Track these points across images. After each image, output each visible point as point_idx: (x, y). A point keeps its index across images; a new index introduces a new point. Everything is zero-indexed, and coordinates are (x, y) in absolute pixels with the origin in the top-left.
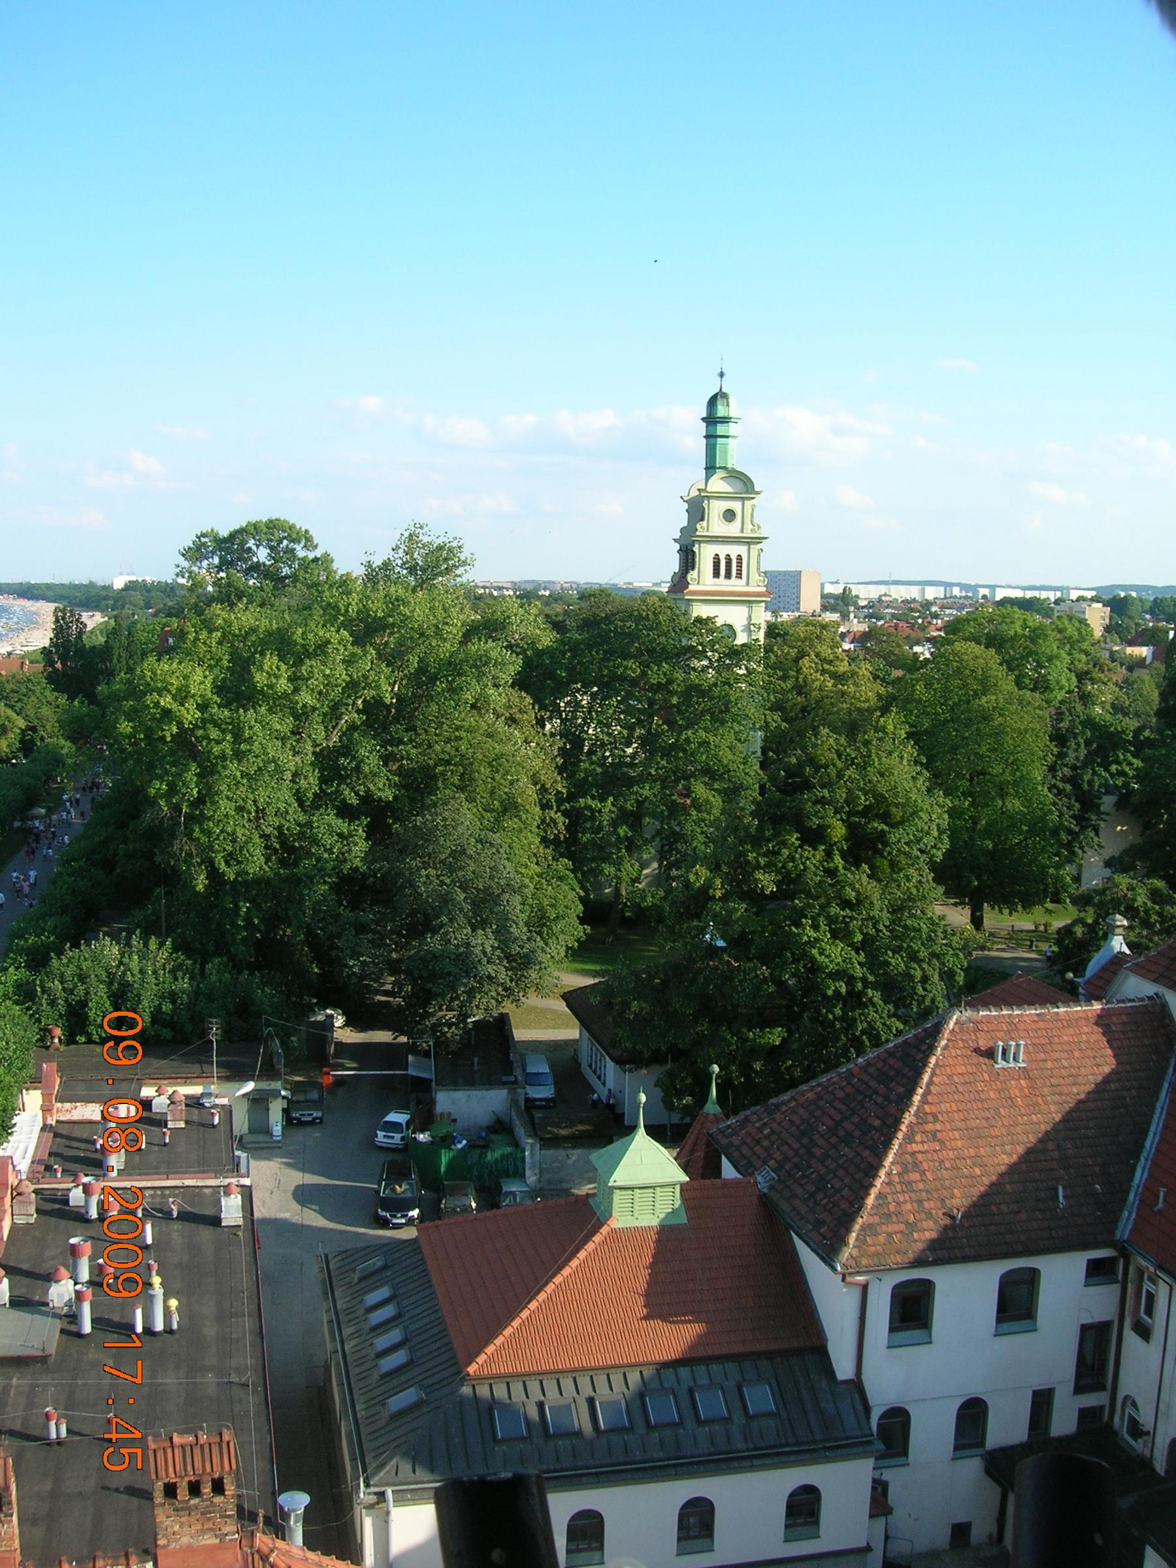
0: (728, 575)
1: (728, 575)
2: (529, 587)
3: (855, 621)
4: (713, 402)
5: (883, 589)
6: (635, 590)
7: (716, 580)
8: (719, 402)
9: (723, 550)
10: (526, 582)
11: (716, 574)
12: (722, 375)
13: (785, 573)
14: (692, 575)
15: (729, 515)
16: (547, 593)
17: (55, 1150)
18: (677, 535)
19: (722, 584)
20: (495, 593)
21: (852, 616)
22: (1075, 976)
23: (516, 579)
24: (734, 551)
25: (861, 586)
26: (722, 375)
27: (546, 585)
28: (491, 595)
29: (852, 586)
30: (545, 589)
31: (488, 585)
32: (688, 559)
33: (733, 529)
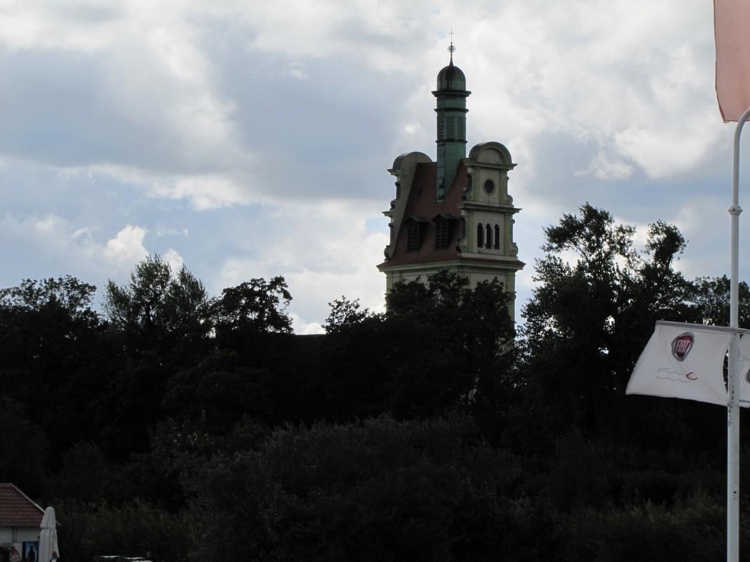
7: (480, 249)
11: (480, 244)
12: (451, 49)
17: (459, 114)
26: (451, 49)
33: (494, 200)
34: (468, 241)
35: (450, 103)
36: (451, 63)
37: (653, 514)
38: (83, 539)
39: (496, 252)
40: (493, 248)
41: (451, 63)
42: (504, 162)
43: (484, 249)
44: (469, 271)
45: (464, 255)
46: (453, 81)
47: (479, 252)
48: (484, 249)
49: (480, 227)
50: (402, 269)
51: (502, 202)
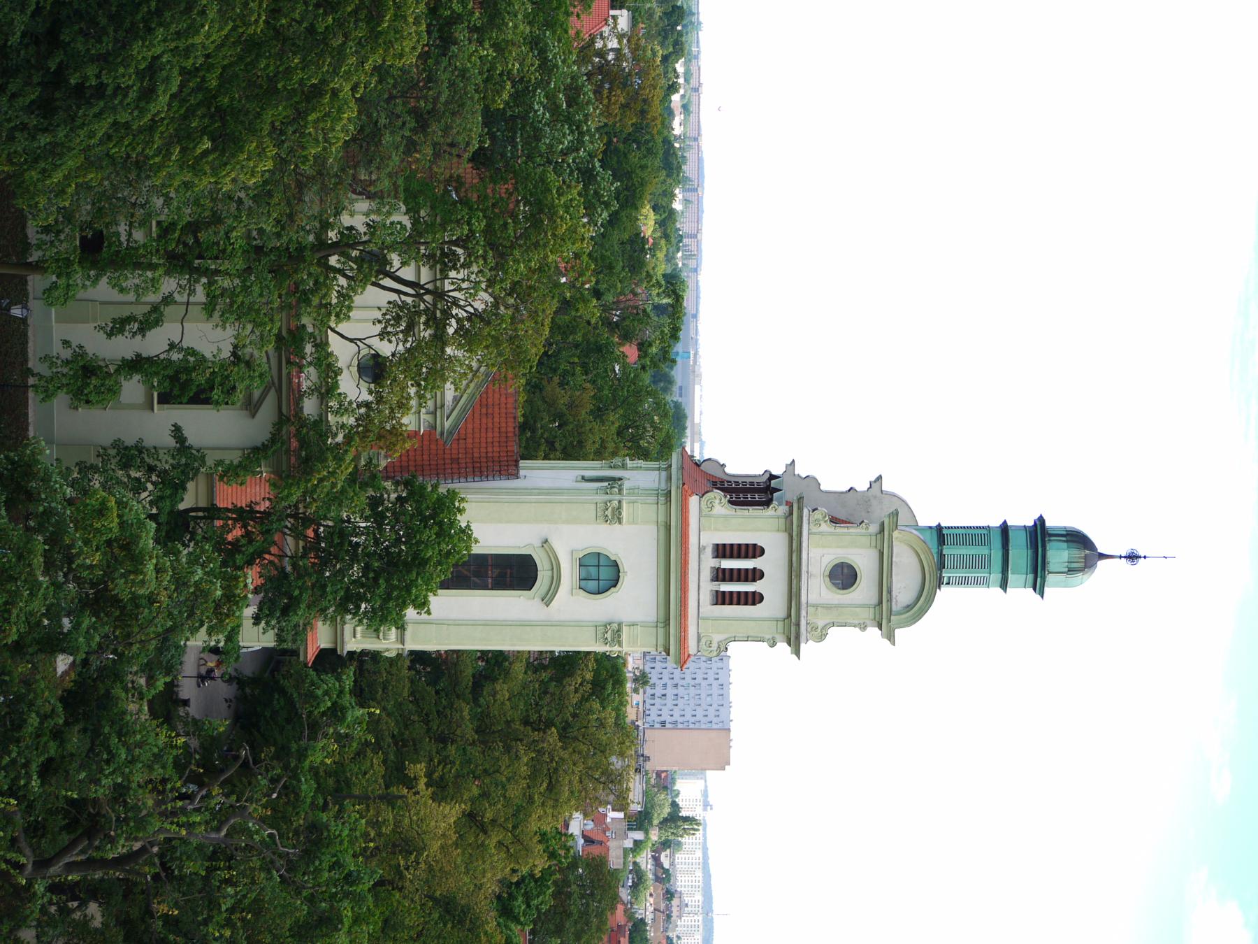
0: (722, 575)
1: (722, 575)
2: (688, 169)
3: (629, 844)
4: (1077, 539)
5: (694, 898)
6: (686, 391)
7: (709, 551)
8: (1078, 553)
9: (772, 563)
10: (700, 160)
11: (723, 551)
12: (1133, 557)
13: (724, 703)
14: (718, 502)
15: (844, 576)
16: (677, 206)
17: (996, 576)
18: (801, 470)
19: (701, 566)
20: (676, 98)
21: (639, 835)
22: (166, 938)
23: (706, 143)
24: (772, 587)
25: (699, 854)
26: (1133, 557)
27: (695, 204)
28: (673, 88)
29: (699, 834)
30: (686, 201)
31: (693, 82)
32: (754, 493)
33: (816, 589)
34: (725, 517)
35: (1020, 554)
36: (1103, 556)
37: (38, 560)
38: (330, 417)
39: (706, 597)
40: (714, 563)
41: (1103, 556)
42: (899, 613)
43: (710, 562)
44: (662, 518)
45: (694, 501)
46: (1065, 545)
47: (701, 549)
48: (710, 562)
49: (754, 551)
50: (673, 532)
51: (811, 610)
